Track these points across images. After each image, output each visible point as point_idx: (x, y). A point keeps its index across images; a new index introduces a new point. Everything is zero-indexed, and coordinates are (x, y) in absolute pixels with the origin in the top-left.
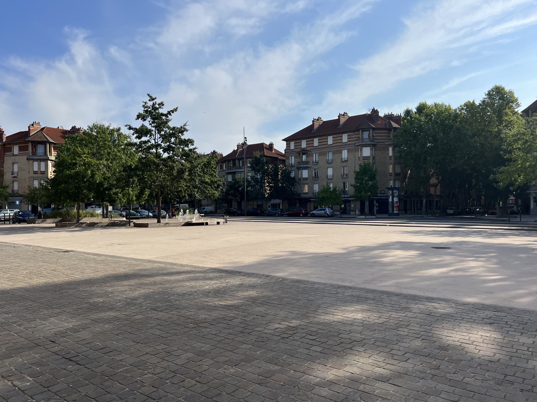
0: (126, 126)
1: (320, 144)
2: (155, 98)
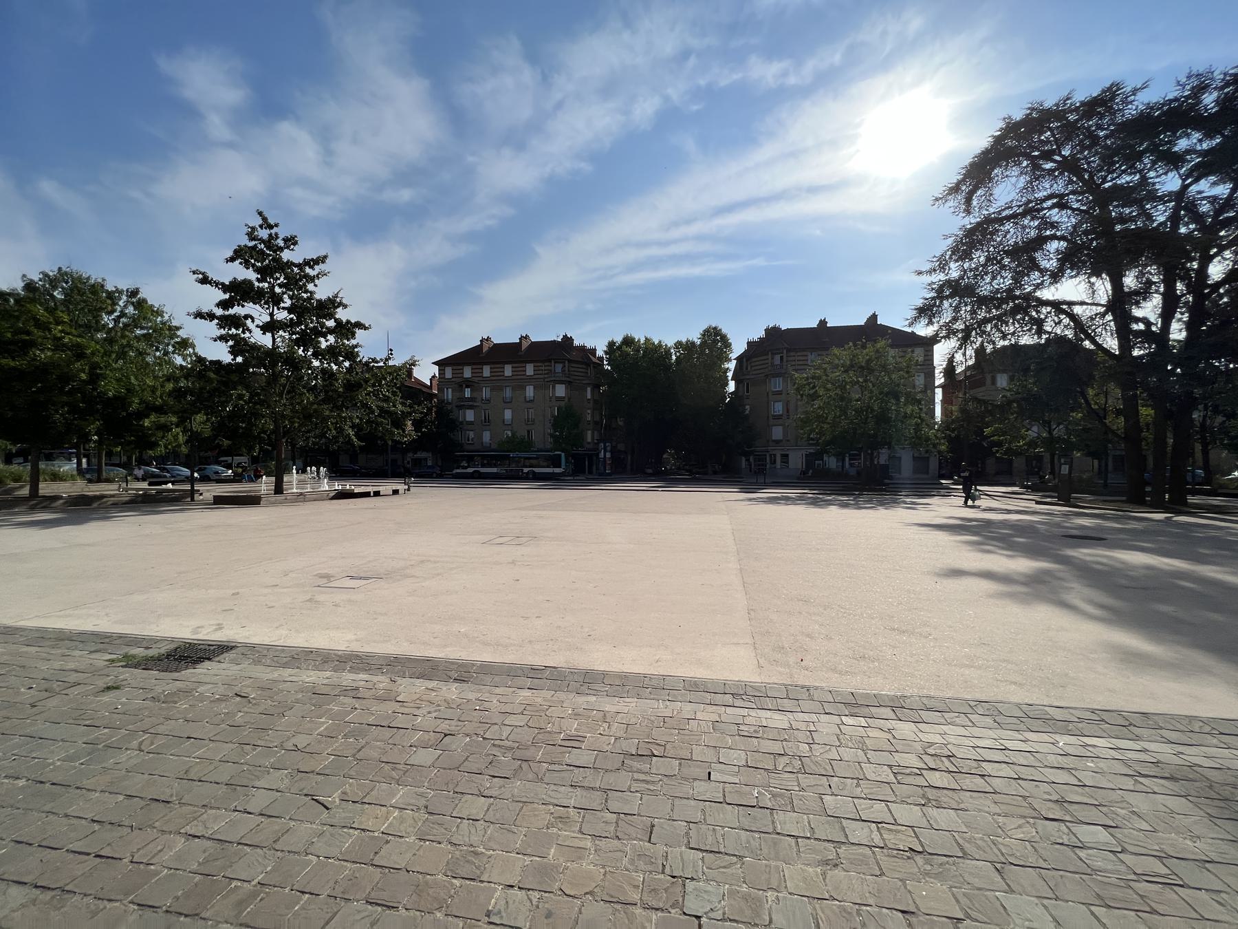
0: (194, 273)
1: (493, 374)
2: (276, 225)
